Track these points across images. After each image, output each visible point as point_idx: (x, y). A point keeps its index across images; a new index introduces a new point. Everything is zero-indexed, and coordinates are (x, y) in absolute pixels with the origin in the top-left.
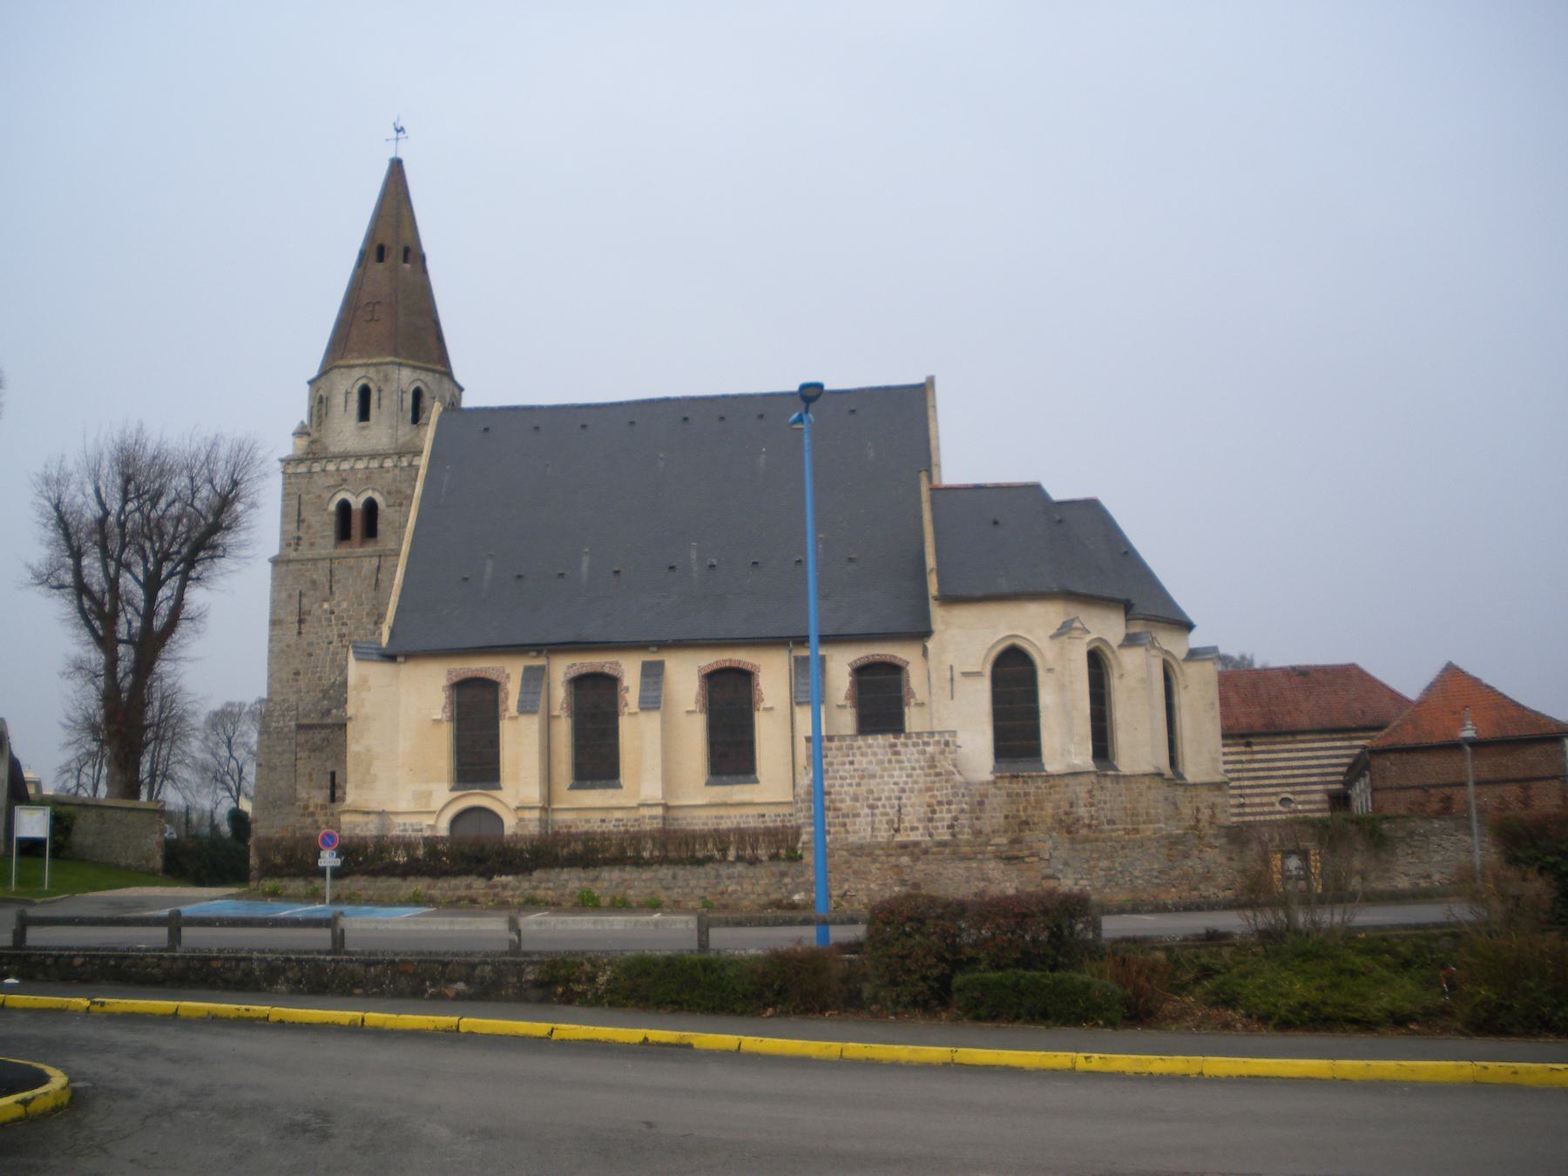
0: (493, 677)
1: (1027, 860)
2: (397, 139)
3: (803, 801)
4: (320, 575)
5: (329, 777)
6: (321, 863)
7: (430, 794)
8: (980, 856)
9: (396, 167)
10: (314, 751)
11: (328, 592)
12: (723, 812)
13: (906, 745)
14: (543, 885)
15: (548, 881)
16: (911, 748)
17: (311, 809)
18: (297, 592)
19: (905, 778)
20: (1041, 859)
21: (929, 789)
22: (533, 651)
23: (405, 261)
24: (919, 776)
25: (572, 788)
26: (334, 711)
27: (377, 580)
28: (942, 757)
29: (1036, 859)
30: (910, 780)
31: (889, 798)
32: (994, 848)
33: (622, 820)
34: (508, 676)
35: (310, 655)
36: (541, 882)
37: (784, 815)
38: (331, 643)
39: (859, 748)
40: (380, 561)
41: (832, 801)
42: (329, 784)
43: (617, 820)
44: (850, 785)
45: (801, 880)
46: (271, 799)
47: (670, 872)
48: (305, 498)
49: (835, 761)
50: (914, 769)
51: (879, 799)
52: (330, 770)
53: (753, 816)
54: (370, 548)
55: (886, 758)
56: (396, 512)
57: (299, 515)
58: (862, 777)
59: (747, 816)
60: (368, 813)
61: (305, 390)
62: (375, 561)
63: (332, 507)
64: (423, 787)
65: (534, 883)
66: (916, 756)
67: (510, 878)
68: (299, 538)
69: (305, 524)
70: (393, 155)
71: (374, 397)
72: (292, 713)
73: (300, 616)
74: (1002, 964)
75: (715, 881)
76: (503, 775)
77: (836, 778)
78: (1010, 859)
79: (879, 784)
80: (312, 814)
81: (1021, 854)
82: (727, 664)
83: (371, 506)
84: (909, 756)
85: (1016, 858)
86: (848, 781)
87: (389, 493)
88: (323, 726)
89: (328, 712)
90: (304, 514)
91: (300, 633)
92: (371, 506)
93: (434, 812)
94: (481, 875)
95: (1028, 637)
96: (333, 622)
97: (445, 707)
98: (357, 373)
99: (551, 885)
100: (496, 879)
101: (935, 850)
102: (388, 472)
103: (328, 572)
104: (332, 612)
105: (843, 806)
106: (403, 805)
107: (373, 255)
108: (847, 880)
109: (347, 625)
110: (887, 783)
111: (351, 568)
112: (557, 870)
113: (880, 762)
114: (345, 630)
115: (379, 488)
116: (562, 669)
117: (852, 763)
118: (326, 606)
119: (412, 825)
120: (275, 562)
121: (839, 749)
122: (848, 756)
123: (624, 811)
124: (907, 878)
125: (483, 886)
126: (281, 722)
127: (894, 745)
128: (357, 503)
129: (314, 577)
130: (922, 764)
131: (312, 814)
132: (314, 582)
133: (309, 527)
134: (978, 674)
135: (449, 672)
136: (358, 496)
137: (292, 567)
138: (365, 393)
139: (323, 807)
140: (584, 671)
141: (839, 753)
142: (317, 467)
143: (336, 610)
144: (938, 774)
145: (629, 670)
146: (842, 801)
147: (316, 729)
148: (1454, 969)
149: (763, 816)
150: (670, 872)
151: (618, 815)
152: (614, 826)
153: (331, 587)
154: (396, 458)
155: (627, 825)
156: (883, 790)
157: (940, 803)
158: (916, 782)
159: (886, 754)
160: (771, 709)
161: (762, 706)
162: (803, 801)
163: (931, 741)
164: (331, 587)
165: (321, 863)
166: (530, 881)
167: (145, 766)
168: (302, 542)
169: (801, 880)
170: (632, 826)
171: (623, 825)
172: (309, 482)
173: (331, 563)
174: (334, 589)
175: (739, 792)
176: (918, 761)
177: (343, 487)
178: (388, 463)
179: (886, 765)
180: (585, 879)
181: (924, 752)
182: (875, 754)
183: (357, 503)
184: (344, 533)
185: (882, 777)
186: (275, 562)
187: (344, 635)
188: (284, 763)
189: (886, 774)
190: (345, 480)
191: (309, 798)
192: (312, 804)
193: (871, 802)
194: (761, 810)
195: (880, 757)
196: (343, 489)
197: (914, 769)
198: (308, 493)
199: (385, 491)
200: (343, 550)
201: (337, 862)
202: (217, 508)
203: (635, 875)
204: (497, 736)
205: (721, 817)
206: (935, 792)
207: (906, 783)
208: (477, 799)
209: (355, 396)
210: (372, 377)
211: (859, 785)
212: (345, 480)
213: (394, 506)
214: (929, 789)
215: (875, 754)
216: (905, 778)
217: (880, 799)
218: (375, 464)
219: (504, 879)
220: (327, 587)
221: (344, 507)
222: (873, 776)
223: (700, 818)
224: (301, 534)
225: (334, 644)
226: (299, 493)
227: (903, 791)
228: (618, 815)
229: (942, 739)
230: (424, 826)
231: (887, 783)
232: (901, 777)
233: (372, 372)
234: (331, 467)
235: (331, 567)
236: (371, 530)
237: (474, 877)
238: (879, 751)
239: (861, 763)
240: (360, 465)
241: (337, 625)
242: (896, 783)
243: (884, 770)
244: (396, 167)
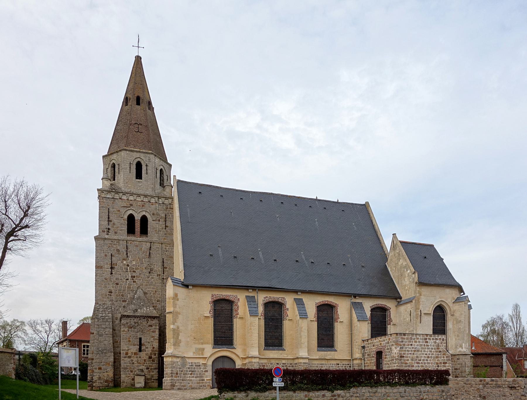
0: (232, 299)
1: (517, 388)
3: (396, 359)
4: (122, 247)
5: (138, 340)
6: (274, 385)
7: (203, 349)
8: (504, 386)
10: (131, 328)
11: (126, 256)
12: (323, 362)
13: (430, 339)
14: (355, 395)
15: (357, 393)
16: (431, 340)
17: (129, 355)
18: (110, 254)
19: (429, 352)
20: (521, 388)
21: (437, 357)
22: (250, 289)
24: (433, 352)
25: (264, 350)
26: (139, 310)
27: (150, 253)
28: (441, 345)
29: (520, 388)
30: (430, 353)
31: (424, 360)
32: (508, 383)
33: (285, 364)
34: (239, 300)
35: (117, 284)
36: (354, 394)
37: (346, 364)
38: (127, 279)
39: (414, 339)
40: (151, 245)
41: (404, 360)
42: (138, 343)
43: (283, 364)
44: (411, 354)
45: (449, 394)
46: (100, 349)
47: (404, 389)
48: (111, 210)
49: (406, 344)
50: (432, 349)
51: (420, 360)
52: (139, 337)
53: (335, 364)
54: (144, 239)
55: (423, 344)
56: (157, 224)
57: (109, 218)
58: (415, 351)
59: (333, 364)
60: (178, 357)
62: (148, 245)
64: (201, 346)
65: (351, 394)
66: (433, 344)
67: (342, 391)
68: (109, 229)
69: (112, 223)
72: (109, 310)
73: (112, 265)
75: (419, 394)
76: (235, 342)
77: (406, 351)
78: (512, 388)
79: (420, 354)
80: (130, 357)
81: (516, 386)
82: (327, 302)
83: (144, 220)
84: (431, 344)
85: (514, 387)
86: (410, 352)
87: (153, 214)
88: (135, 317)
89: (137, 310)
90: (111, 218)
91: (112, 273)
93: (207, 358)
94: (328, 390)
95: (446, 301)
96: (129, 270)
97: (210, 311)
98: (138, 155)
99: (358, 395)
100: (336, 392)
101: (491, 383)
102: (153, 205)
103: (126, 247)
104: (128, 265)
105: (408, 362)
106: (191, 355)
107: (132, 102)
108: (463, 394)
109: (135, 272)
110: (423, 354)
111: (137, 246)
112: (360, 388)
113: (421, 345)
114: (134, 274)
115: (148, 211)
116: (262, 298)
117: (411, 345)
118: (125, 262)
119: (195, 363)
120: (96, 238)
121: (407, 339)
122: (410, 342)
123: (286, 360)
124: (482, 394)
125: (330, 395)
126: (104, 314)
127: (426, 339)
129: (118, 248)
130: (435, 347)
131: (130, 357)
132: (118, 250)
133: (114, 224)
134: (430, 314)
135: (212, 296)
137: (106, 242)
139: (135, 354)
140: (271, 300)
141: (407, 340)
142: (117, 196)
143: (130, 264)
144: (440, 352)
145: (289, 301)
146: (408, 360)
147: (132, 317)
149: (338, 364)
150: (404, 389)
151: (284, 362)
152: (282, 366)
153: (127, 254)
154: (157, 198)
155: (287, 366)
156: (422, 357)
157: (441, 363)
158: (433, 354)
159: (423, 342)
160: (342, 322)
161: (339, 320)
162: (396, 359)
163: (438, 338)
164: (127, 254)
165: (274, 385)
166: (349, 393)
168: (110, 231)
169: (449, 394)
170: (289, 366)
171: (286, 366)
172: (113, 203)
173: (127, 243)
174: (128, 255)
175: (328, 354)
176: (434, 346)
177: (131, 208)
178: (153, 201)
179: (423, 347)
180: (372, 392)
181: (435, 342)
182: (419, 342)
184: (131, 230)
185: (421, 351)
186: (96, 238)
187: (134, 277)
188: (106, 333)
189: (423, 350)
190: (131, 205)
191: (128, 350)
192: (129, 352)
193: (418, 361)
194: (338, 362)
195: (421, 343)
196: (131, 209)
197: (432, 349)
198: (113, 208)
199: (151, 213)
200: (131, 238)
201: (282, 384)
203: (391, 391)
204: (232, 325)
205: (323, 364)
206: (439, 359)
207: (429, 354)
208: (224, 352)
209: (134, 167)
211: (413, 354)
212: (131, 205)
213: (156, 221)
214: (437, 357)
215: (419, 342)
216: (429, 352)
217: (420, 360)
218: (146, 200)
219: (339, 392)
220: (125, 253)
222: (418, 351)
223: (315, 364)
224: (109, 227)
225: (129, 280)
226: (108, 207)
227: (428, 357)
228: (284, 362)
229: (442, 338)
230: (201, 364)
231: (423, 354)
232: (428, 352)
234: (124, 197)
235: (127, 245)
236: (144, 231)
237: (326, 391)
238: (421, 341)
239: (414, 345)
240: (139, 199)
241: (130, 271)
242: (426, 354)
243: (422, 348)
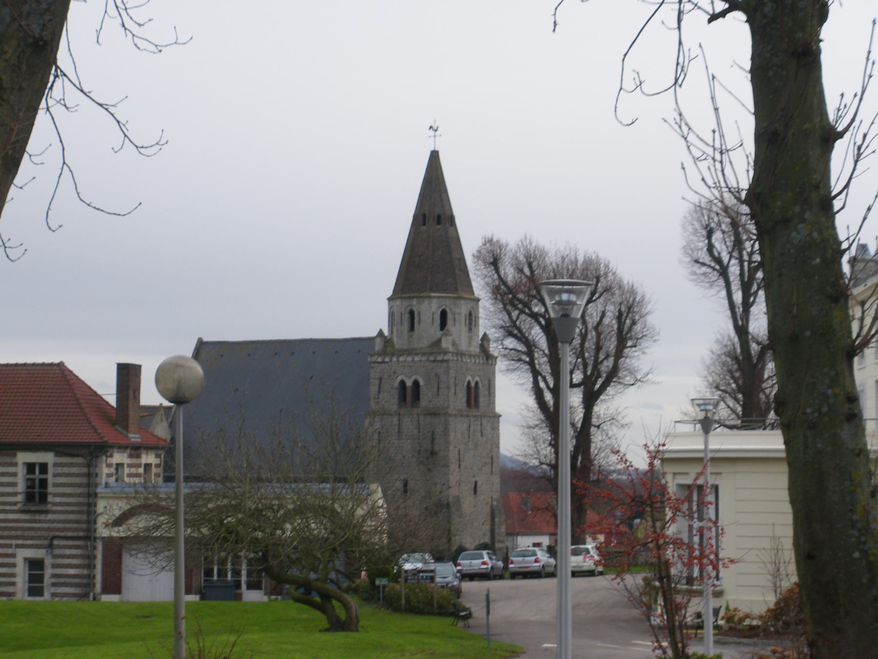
2: (435, 136)
9: (434, 157)
23: (424, 224)
61: (386, 303)
63: (396, 383)
70: (433, 149)
71: (450, 316)
74: (302, 590)
83: (416, 384)
92: (416, 384)
128: (409, 383)
136: (410, 378)
138: (444, 315)
148: (363, 573)
167: (665, 617)
183: (409, 383)
202: (542, 417)
209: (437, 317)
210: (448, 305)
221: (403, 383)
233: (448, 302)
244: (434, 157)
